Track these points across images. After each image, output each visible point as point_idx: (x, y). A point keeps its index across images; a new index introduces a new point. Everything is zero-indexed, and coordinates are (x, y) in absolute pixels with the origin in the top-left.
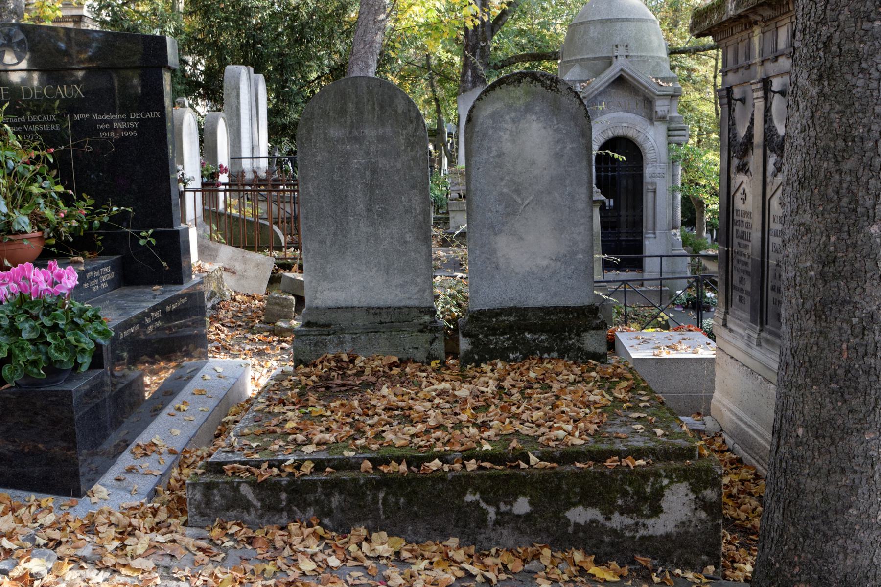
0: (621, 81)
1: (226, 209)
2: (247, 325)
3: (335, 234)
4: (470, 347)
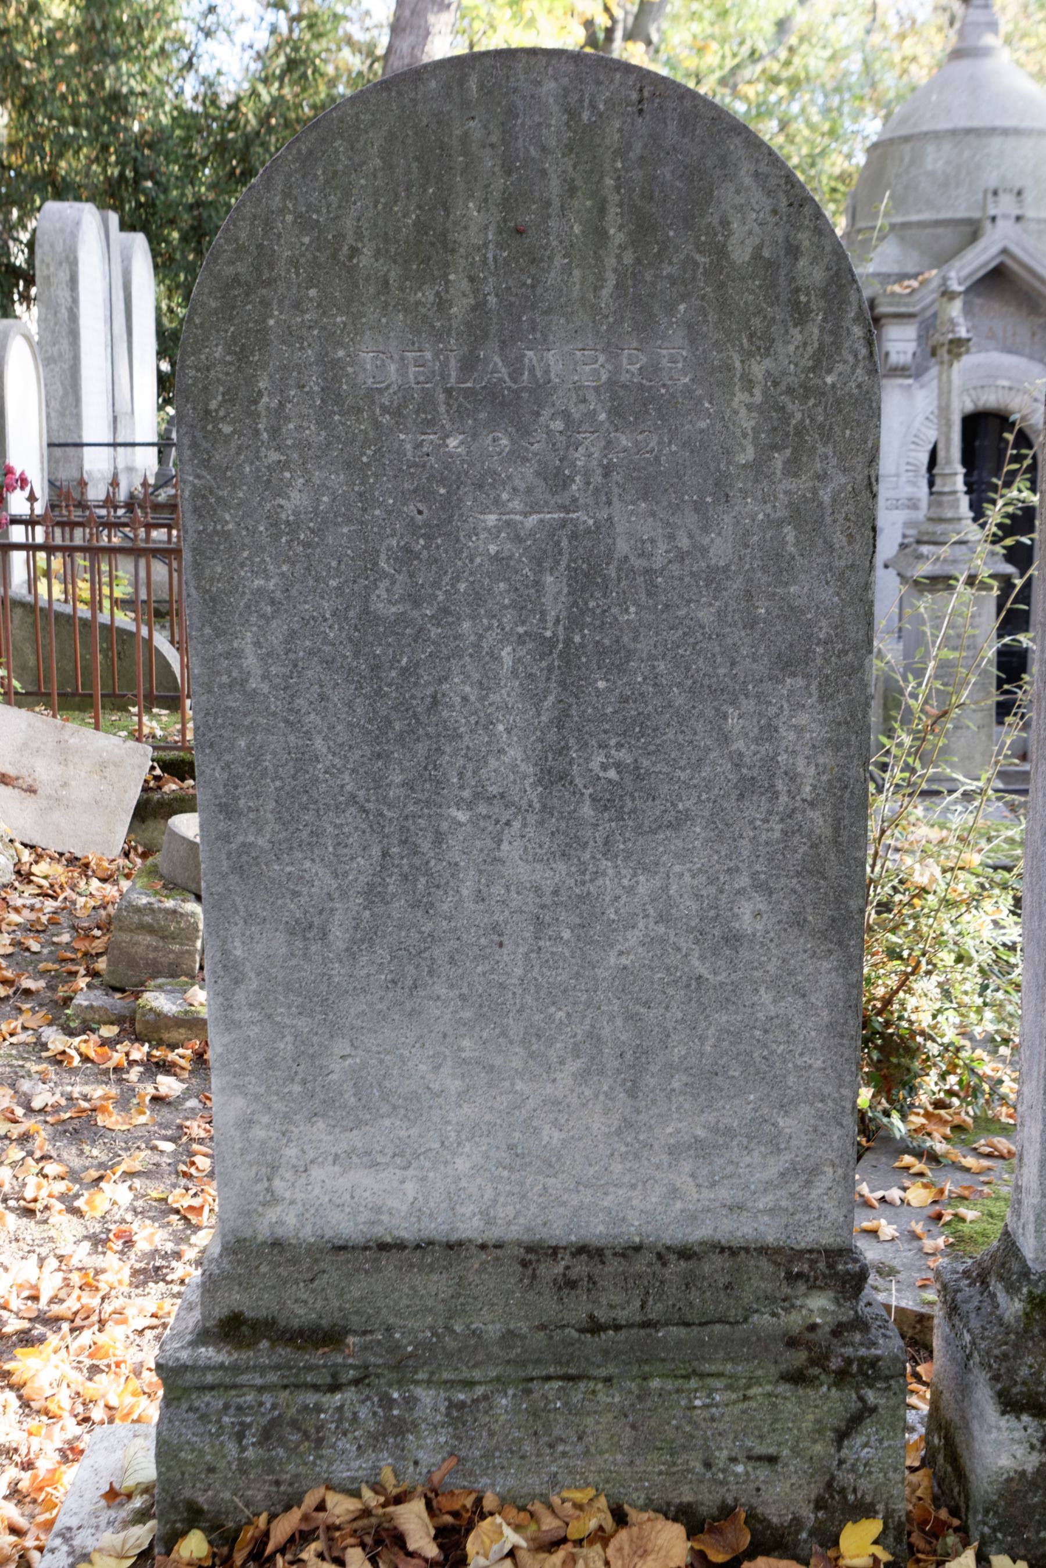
0: (999, 280)
1: (32, 584)
2: (51, 988)
3: (373, 894)
4: (1031, 1462)
